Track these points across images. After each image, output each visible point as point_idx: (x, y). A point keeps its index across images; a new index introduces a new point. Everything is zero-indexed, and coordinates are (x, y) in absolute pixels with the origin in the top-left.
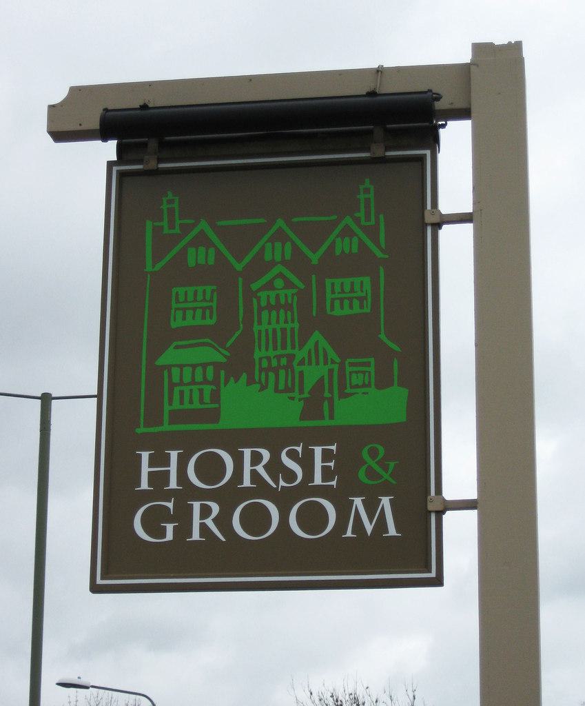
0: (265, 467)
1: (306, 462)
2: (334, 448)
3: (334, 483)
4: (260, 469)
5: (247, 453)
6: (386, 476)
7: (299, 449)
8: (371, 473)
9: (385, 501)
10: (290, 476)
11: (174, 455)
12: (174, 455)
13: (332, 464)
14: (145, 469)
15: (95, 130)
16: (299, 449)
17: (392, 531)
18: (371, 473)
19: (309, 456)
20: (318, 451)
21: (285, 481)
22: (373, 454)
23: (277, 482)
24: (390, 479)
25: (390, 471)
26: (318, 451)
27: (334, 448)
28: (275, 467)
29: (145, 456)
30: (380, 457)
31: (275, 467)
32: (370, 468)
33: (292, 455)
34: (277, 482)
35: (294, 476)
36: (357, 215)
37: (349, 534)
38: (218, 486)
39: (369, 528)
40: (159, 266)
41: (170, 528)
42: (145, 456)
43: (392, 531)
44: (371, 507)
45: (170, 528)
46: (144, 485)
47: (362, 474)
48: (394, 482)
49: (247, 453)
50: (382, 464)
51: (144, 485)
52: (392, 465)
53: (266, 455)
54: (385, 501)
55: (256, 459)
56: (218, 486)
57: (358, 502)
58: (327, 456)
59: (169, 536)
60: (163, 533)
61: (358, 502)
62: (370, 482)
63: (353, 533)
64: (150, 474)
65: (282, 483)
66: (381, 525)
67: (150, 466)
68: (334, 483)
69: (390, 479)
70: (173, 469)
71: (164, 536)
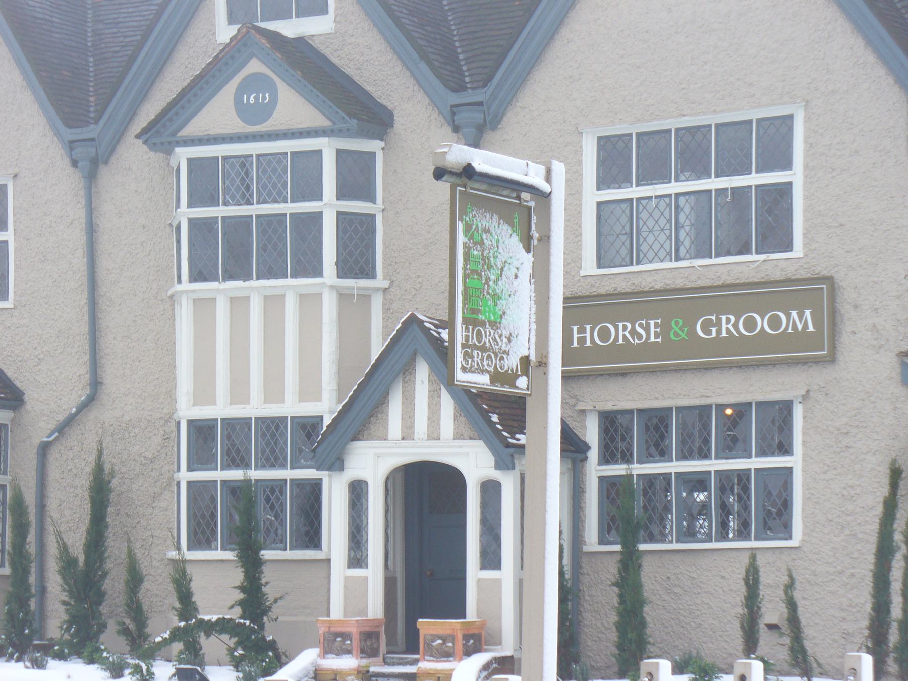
1: (647, 329)
2: (659, 321)
3: (660, 340)
5: (620, 325)
6: (683, 336)
7: (644, 322)
8: (676, 334)
9: (807, 313)
10: (640, 337)
11: (588, 327)
12: (588, 327)
14: (575, 336)
15: (209, 665)
16: (644, 322)
17: (811, 329)
18: (676, 334)
19: (648, 325)
20: (652, 323)
21: (638, 340)
22: (677, 323)
23: (634, 341)
24: (685, 337)
26: (652, 323)
27: (659, 321)
28: (633, 333)
29: (575, 328)
31: (633, 333)
32: (675, 331)
33: (641, 326)
34: (634, 341)
36: (171, 489)
37: (790, 331)
38: (609, 343)
39: (800, 327)
40: (490, 118)
41: (714, 330)
42: (575, 328)
43: (811, 329)
44: (801, 315)
45: (714, 330)
46: (575, 344)
48: (687, 339)
49: (620, 325)
50: (681, 329)
51: (575, 344)
52: (686, 329)
53: (629, 326)
54: (807, 313)
55: (625, 328)
56: (609, 343)
57: (794, 313)
58: (656, 325)
59: (714, 335)
60: (710, 334)
61: (794, 313)
64: (577, 338)
65: (637, 341)
66: (805, 326)
67: (578, 334)
68: (660, 340)
69: (685, 337)
70: (588, 335)
71: (711, 335)
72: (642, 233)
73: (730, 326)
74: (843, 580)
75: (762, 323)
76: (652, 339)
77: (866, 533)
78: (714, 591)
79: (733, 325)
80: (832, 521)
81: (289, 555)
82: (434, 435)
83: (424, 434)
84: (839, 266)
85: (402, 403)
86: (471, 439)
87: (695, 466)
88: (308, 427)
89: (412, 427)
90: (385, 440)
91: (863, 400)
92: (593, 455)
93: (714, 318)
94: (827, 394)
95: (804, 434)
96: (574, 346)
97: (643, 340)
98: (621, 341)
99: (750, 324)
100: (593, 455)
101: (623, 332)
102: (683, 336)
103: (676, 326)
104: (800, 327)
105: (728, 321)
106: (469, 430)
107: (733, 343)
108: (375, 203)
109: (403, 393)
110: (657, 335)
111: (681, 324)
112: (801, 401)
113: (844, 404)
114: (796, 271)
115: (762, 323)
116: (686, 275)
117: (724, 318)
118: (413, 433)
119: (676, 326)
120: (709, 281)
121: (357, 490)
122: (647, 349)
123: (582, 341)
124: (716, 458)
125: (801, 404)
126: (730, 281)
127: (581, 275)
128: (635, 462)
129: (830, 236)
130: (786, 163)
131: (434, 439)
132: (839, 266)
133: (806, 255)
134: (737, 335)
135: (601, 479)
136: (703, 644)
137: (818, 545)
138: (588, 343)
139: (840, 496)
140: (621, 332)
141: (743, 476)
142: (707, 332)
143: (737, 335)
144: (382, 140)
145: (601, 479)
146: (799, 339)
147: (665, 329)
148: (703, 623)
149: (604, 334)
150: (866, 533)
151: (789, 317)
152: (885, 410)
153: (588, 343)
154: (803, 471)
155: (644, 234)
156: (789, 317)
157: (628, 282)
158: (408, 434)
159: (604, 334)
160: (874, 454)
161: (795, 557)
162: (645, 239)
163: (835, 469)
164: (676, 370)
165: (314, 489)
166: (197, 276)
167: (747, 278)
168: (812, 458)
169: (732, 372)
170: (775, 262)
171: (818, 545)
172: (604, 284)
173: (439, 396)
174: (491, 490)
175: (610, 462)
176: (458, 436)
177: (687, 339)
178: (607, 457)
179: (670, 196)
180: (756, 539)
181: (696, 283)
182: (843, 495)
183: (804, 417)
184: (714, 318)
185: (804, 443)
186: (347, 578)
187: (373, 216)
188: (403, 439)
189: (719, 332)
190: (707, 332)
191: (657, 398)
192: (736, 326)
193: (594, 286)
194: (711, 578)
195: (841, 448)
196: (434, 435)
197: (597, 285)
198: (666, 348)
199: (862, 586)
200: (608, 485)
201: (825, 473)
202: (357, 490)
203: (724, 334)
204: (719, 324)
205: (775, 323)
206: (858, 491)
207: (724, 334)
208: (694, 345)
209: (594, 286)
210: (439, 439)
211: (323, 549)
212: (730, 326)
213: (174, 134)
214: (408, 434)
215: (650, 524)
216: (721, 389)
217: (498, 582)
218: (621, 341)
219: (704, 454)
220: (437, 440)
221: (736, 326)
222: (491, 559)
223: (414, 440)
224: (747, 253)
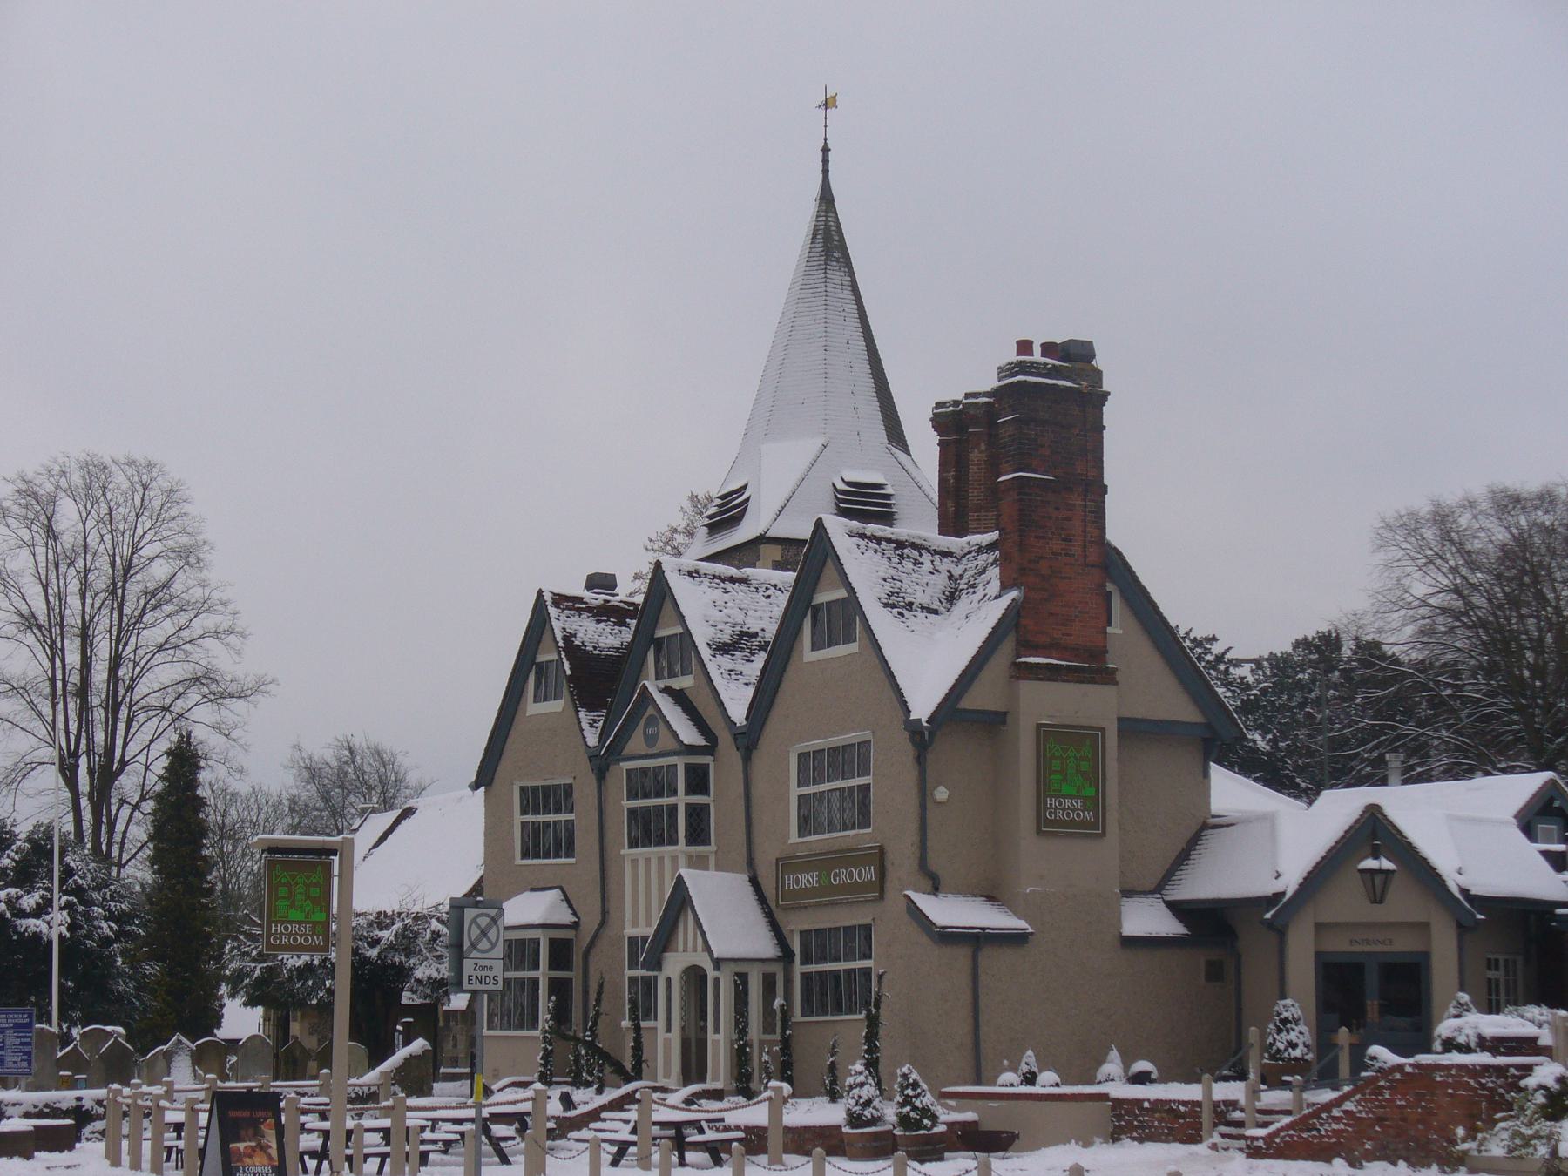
1: (305, 928)
28: (299, 929)
92: (797, 959)
98: (803, 886)
100: (797, 959)
108: (709, 796)
121: (669, 980)
135: (802, 974)
142: (835, 880)
144: (712, 755)
145: (802, 974)
165: (656, 977)
166: (633, 844)
174: (717, 981)
178: (806, 960)
179: (839, 789)
187: (709, 805)
190: (835, 880)
200: (806, 977)
202: (669, 980)
203: (283, 943)
207: (841, 882)
211: (1282, 890)
213: (619, 754)
215: (1545, 854)
222: (717, 1030)
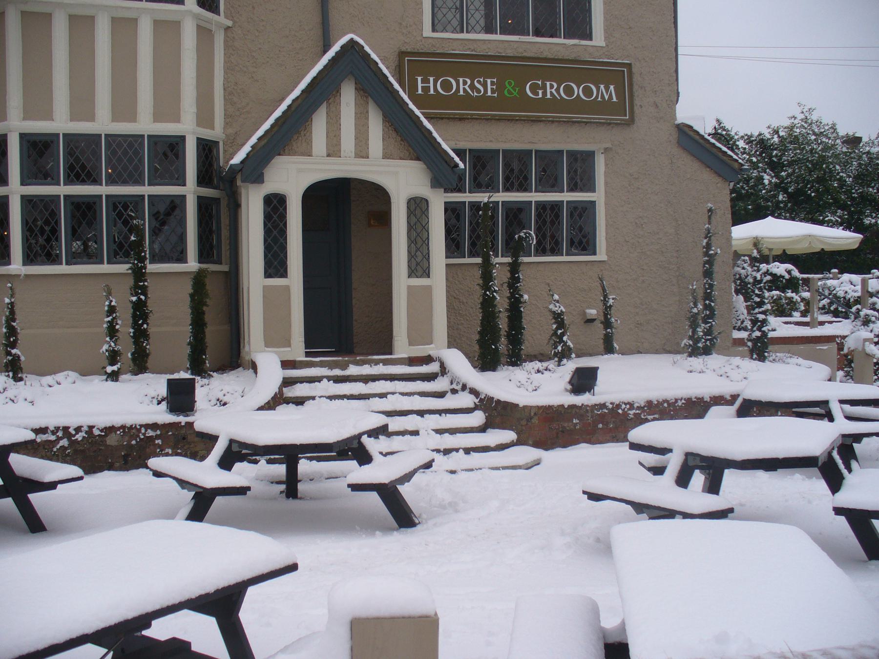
0: (468, 86)
1: (485, 85)
2: (495, 80)
3: (496, 95)
4: (466, 87)
6: (515, 94)
7: (482, 80)
8: (509, 92)
9: (612, 87)
10: (479, 91)
11: (431, 79)
12: (431, 79)
13: (495, 87)
14: (420, 85)
16: (482, 80)
17: (615, 99)
18: (509, 92)
21: (477, 93)
22: (510, 84)
24: (517, 95)
25: (516, 92)
26: (489, 81)
28: (472, 87)
29: (419, 79)
30: (513, 85)
31: (472, 87)
33: (479, 82)
35: (480, 92)
37: (599, 99)
38: (451, 93)
39: (607, 98)
41: (540, 92)
42: (419, 79)
43: (615, 99)
44: (607, 89)
45: (540, 92)
46: (420, 92)
47: (506, 92)
48: (518, 96)
49: (461, 80)
51: (420, 92)
52: (517, 89)
54: (612, 87)
55: (465, 83)
56: (451, 93)
57: (602, 87)
58: (492, 83)
59: (540, 96)
61: (602, 87)
62: (509, 96)
63: (601, 99)
65: (475, 94)
66: (611, 96)
68: (496, 95)
69: (517, 95)
71: (539, 96)
72: (470, 11)
73: (553, 91)
74: (636, 285)
75: (578, 91)
76: (489, 93)
77: (652, 251)
78: (540, 295)
79: (555, 90)
80: (628, 242)
81: (565, 258)
82: (362, 152)
83: (351, 152)
84: (629, 57)
85: (327, 123)
86: (401, 159)
87: (516, 196)
88: (40, 144)
89: (339, 144)
90: (309, 156)
91: (649, 155)
93: (540, 83)
94: (624, 149)
95: (605, 176)
96: (431, 93)
97: (481, 94)
98: (462, 93)
99: (569, 91)
101: (463, 85)
102: (515, 94)
103: (510, 87)
104: (607, 98)
105: (552, 87)
106: (399, 151)
107: (555, 104)
109: (327, 113)
110: (493, 91)
111: (513, 85)
112: (603, 152)
113: (636, 157)
114: (600, 56)
115: (578, 91)
116: (515, 47)
117: (548, 84)
118: (340, 151)
119: (510, 87)
120: (534, 54)
122: (483, 102)
123: (426, 89)
124: (536, 191)
125: (603, 155)
126: (550, 56)
127: (424, 36)
128: (467, 192)
129: (623, 34)
130: (590, 187)
131: (363, 157)
132: (629, 57)
133: (607, 46)
134: (559, 98)
136: (533, 336)
137: (619, 259)
138: (432, 92)
139: (634, 224)
140: (462, 86)
141: (556, 206)
143: (559, 98)
146: (604, 107)
147: (500, 87)
148: (532, 320)
149: (447, 86)
150: (652, 251)
151: (598, 89)
152: (664, 163)
153: (432, 92)
154: (605, 204)
155: (472, 12)
156: (598, 89)
157: (464, 47)
158: (333, 150)
159: (447, 86)
160: (657, 195)
161: (602, 268)
162: (472, 16)
163: (629, 204)
164: (509, 120)
167: (563, 56)
168: (612, 195)
169: (554, 126)
170: (585, 47)
171: (619, 259)
172: (443, 45)
173: (367, 119)
175: (510, 190)
176: (385, 156)
177: (518, 96)
180: (567, 254)
181: (523, 55)
182: (636, 223)
183: (606, 165)
184: (540, 83)
185: (606, 183)
186: (409, 288)
188: (328, 155)
189: (545, 93)
191: (491, 141)
192: (558, 90)
193: (435, 47)
194: (537, 284)
195: (633, 189)
196: (362, 152)
197: (438, 46)
198: (500, 102)
199: (650, 290)
201: (622, 206)
203: (549, 96)
204: (544, 88)
205: (588, 92)
206: (646, 221)
207: (549, 96)
208: (525, 103)
209: (435, 47)
210: (368, 158)
212: (553, 91)
214: (333, 150)
216: (545, 138)
217: (287, 288)
218: (462, 93)
219: (524, 187)
220: (365, 158)
221: (558, 90)
223: (340, 157)
224: (556, 37)
